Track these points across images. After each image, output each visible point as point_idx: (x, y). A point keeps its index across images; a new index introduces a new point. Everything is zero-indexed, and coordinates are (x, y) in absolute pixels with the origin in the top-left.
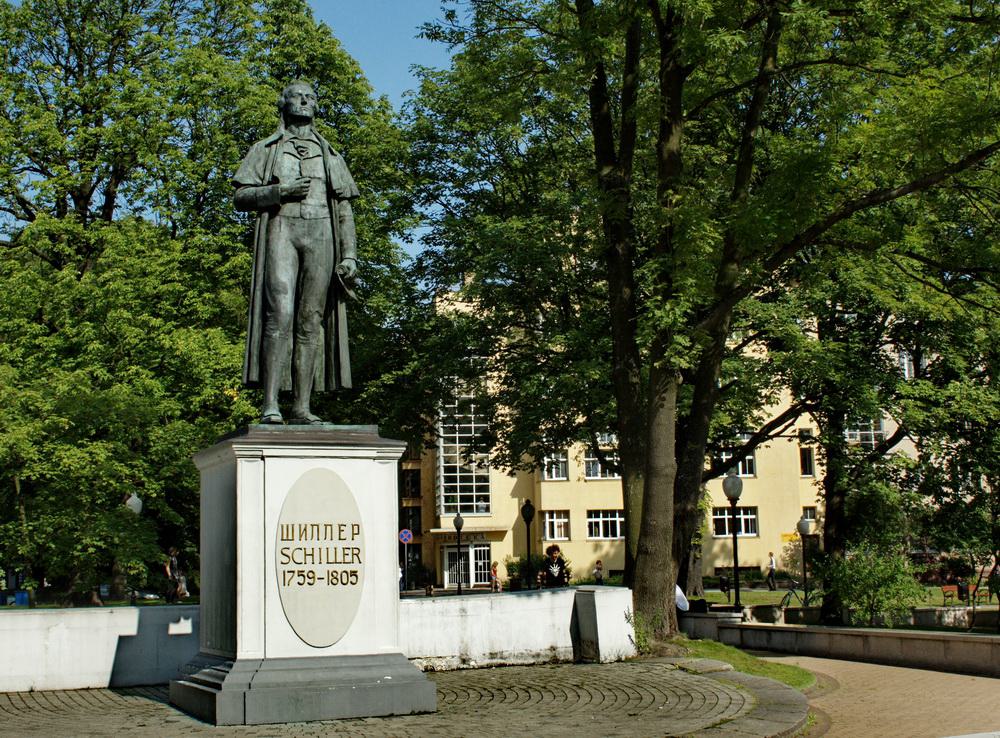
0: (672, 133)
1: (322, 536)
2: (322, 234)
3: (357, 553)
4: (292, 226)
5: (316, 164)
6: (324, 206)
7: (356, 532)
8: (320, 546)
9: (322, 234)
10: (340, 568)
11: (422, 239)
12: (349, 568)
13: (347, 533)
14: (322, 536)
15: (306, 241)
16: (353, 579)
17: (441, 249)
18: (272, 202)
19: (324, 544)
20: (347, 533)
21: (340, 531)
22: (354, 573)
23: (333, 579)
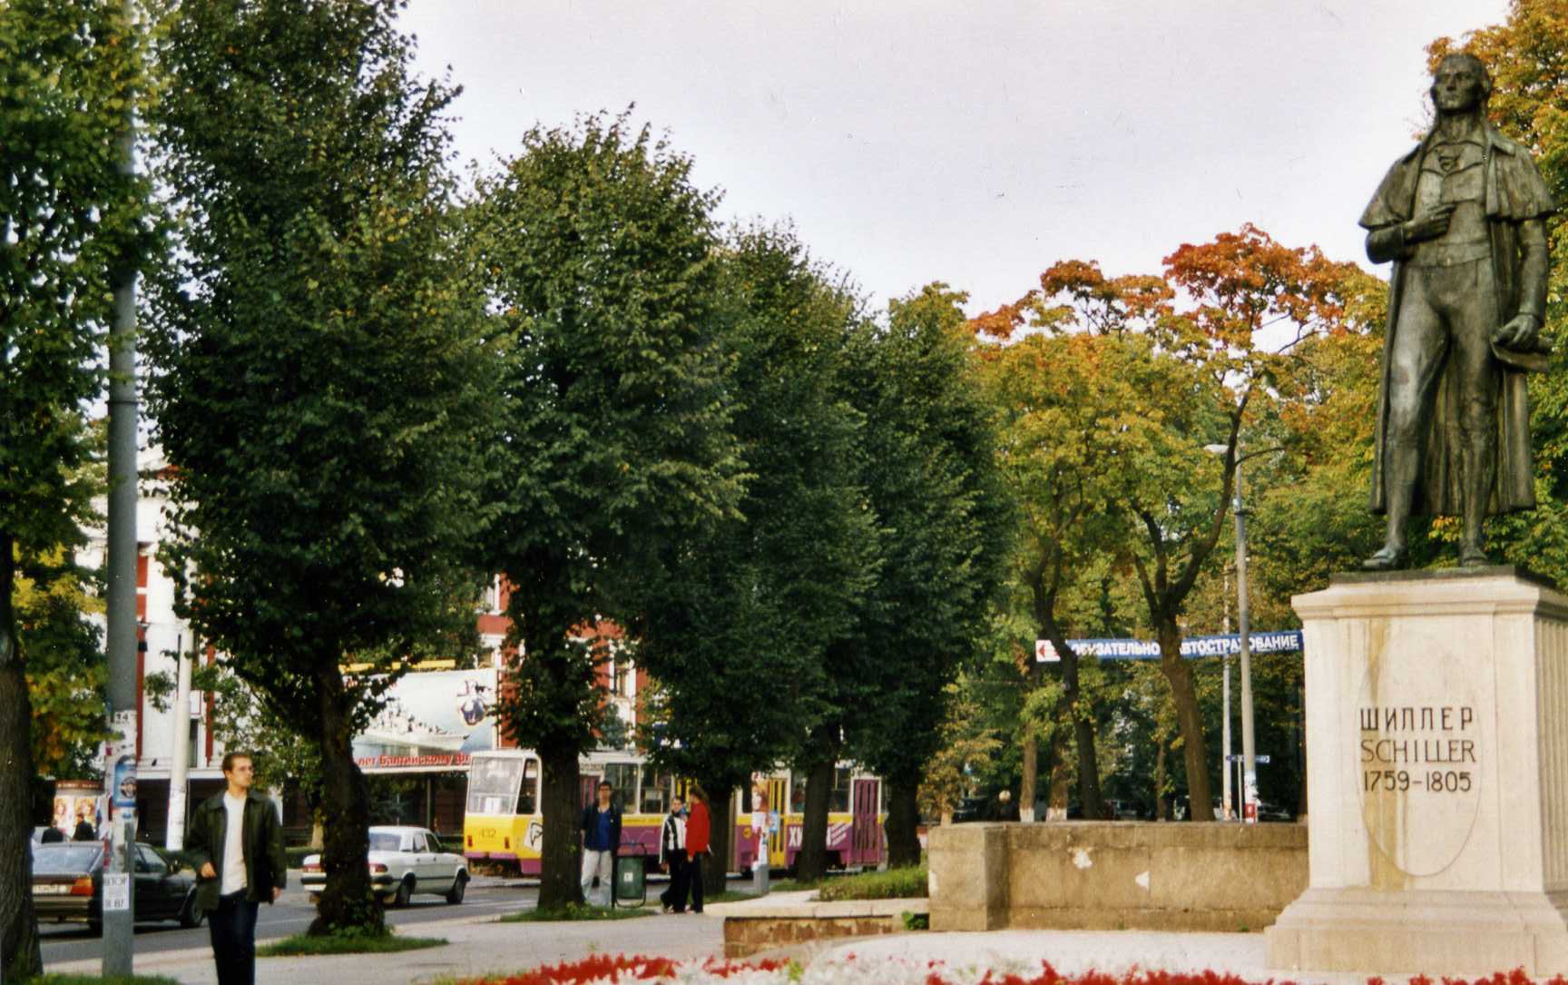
0: (1259, 797)
1: (1418, 723)
2: (1476, 284)
3: (1468, 749)
4: (1426, 281)
5: (1471, 178)
6: (1479, 242)
7: (1467, 717)
8: (1446, 704)
9: (1476, 284)
10: (1444, 769)
11: (687, 168)
12: (1458, 769)
13: (1454, 720)
14: (1418, 723)
15: (1449, 299)
16: (1464, 783)
17: (431, 196)
18: (93, 356)
19: (1420, 735)
20: (1454, 720)
21: (1444, 717)
22: (1464, 776)
23: (1436, 782)
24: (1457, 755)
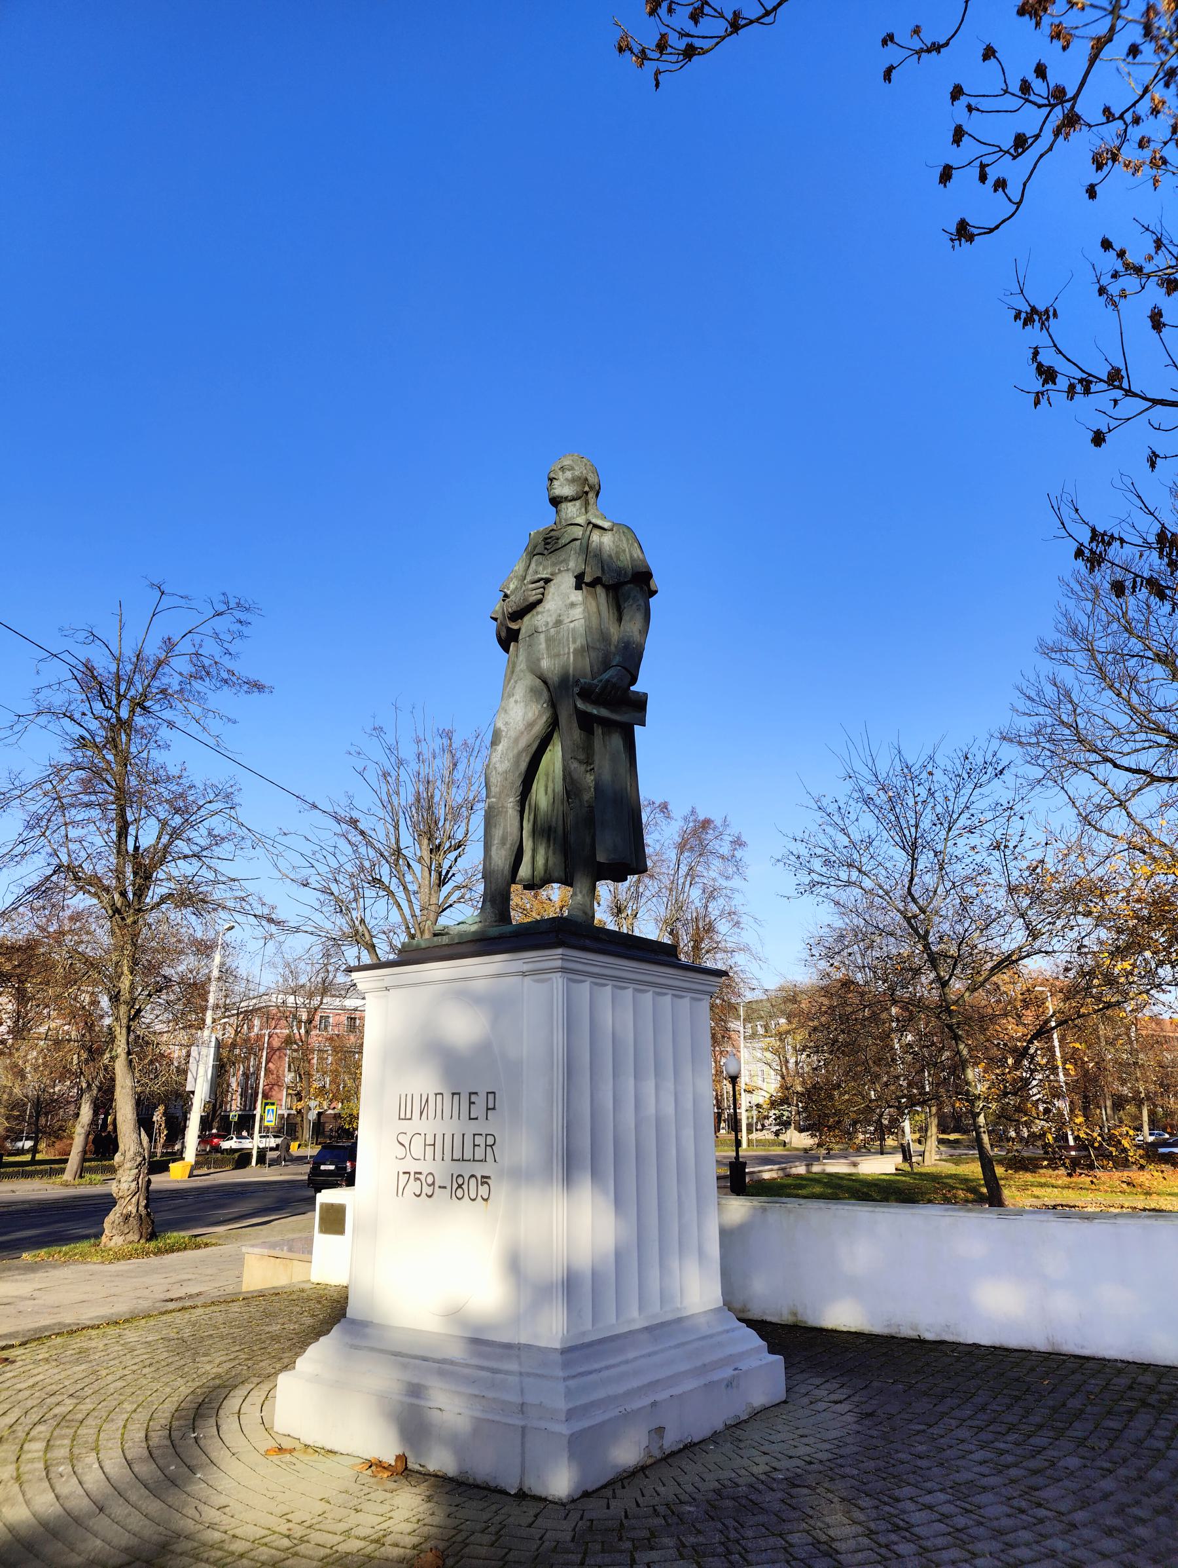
24: (479, 1153)
